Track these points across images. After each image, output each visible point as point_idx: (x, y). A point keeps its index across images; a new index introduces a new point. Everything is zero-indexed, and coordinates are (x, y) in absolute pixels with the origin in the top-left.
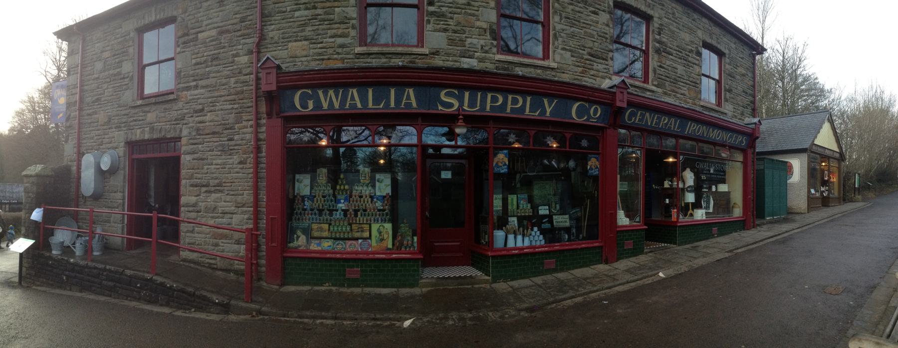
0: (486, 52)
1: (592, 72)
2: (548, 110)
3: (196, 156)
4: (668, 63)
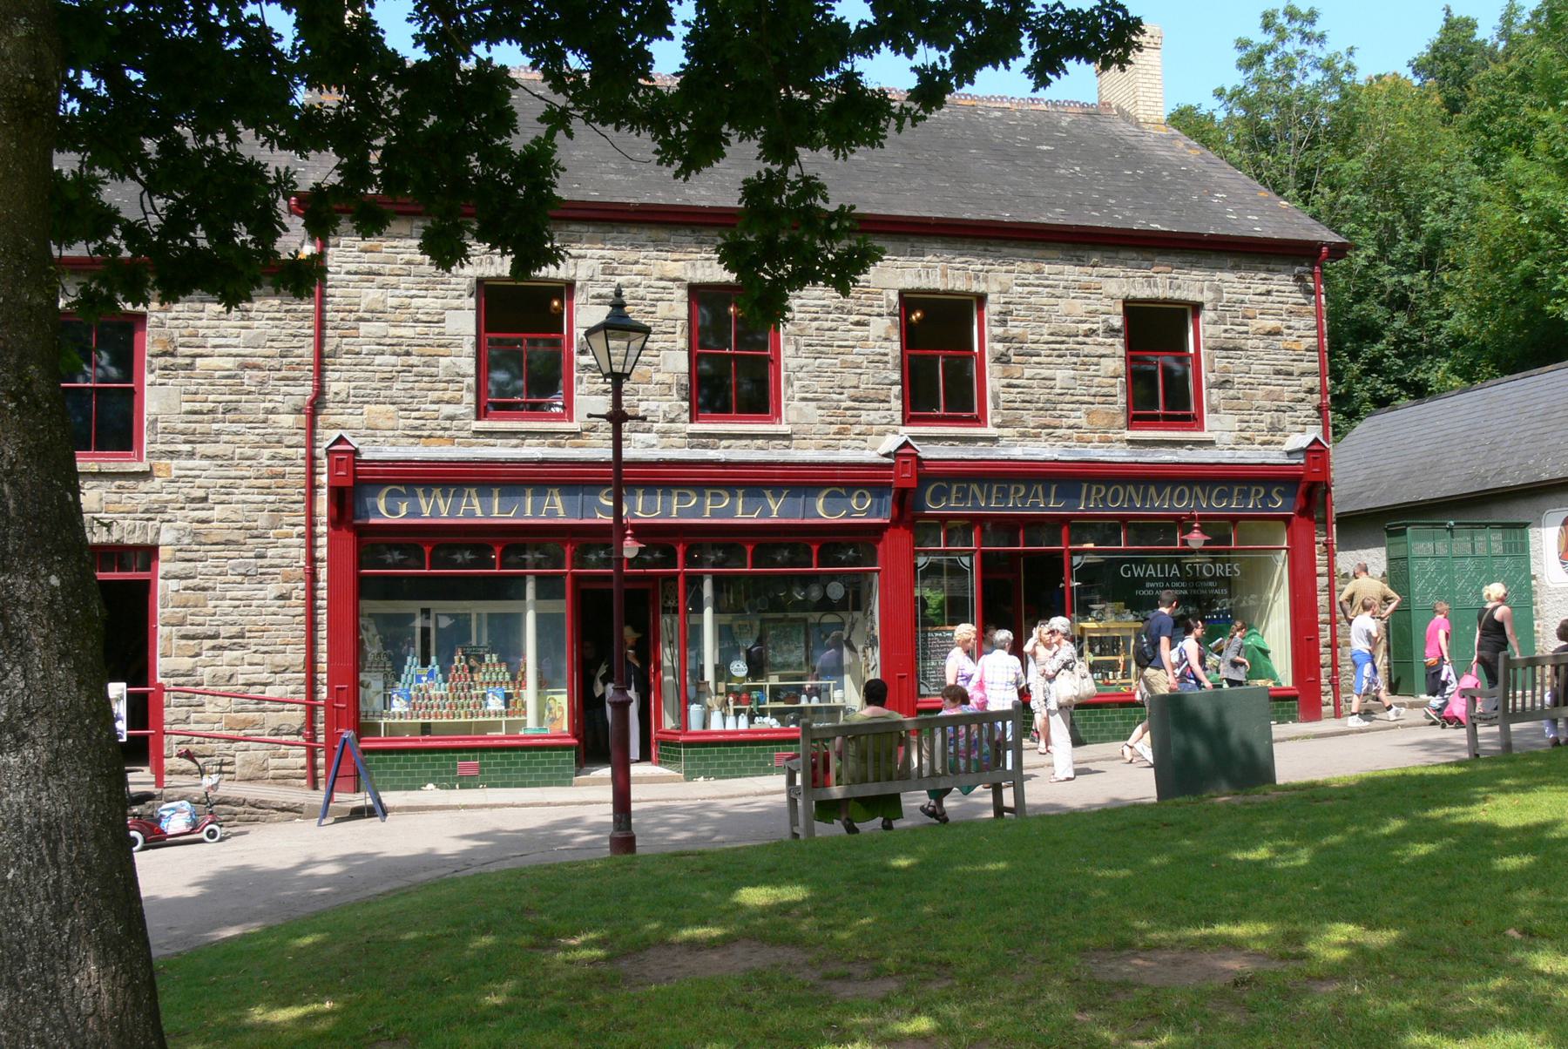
0: (672, 421)
1: (858, 428)
2: (775, 509)
3: (190, 583)
4: (1028, 373)
